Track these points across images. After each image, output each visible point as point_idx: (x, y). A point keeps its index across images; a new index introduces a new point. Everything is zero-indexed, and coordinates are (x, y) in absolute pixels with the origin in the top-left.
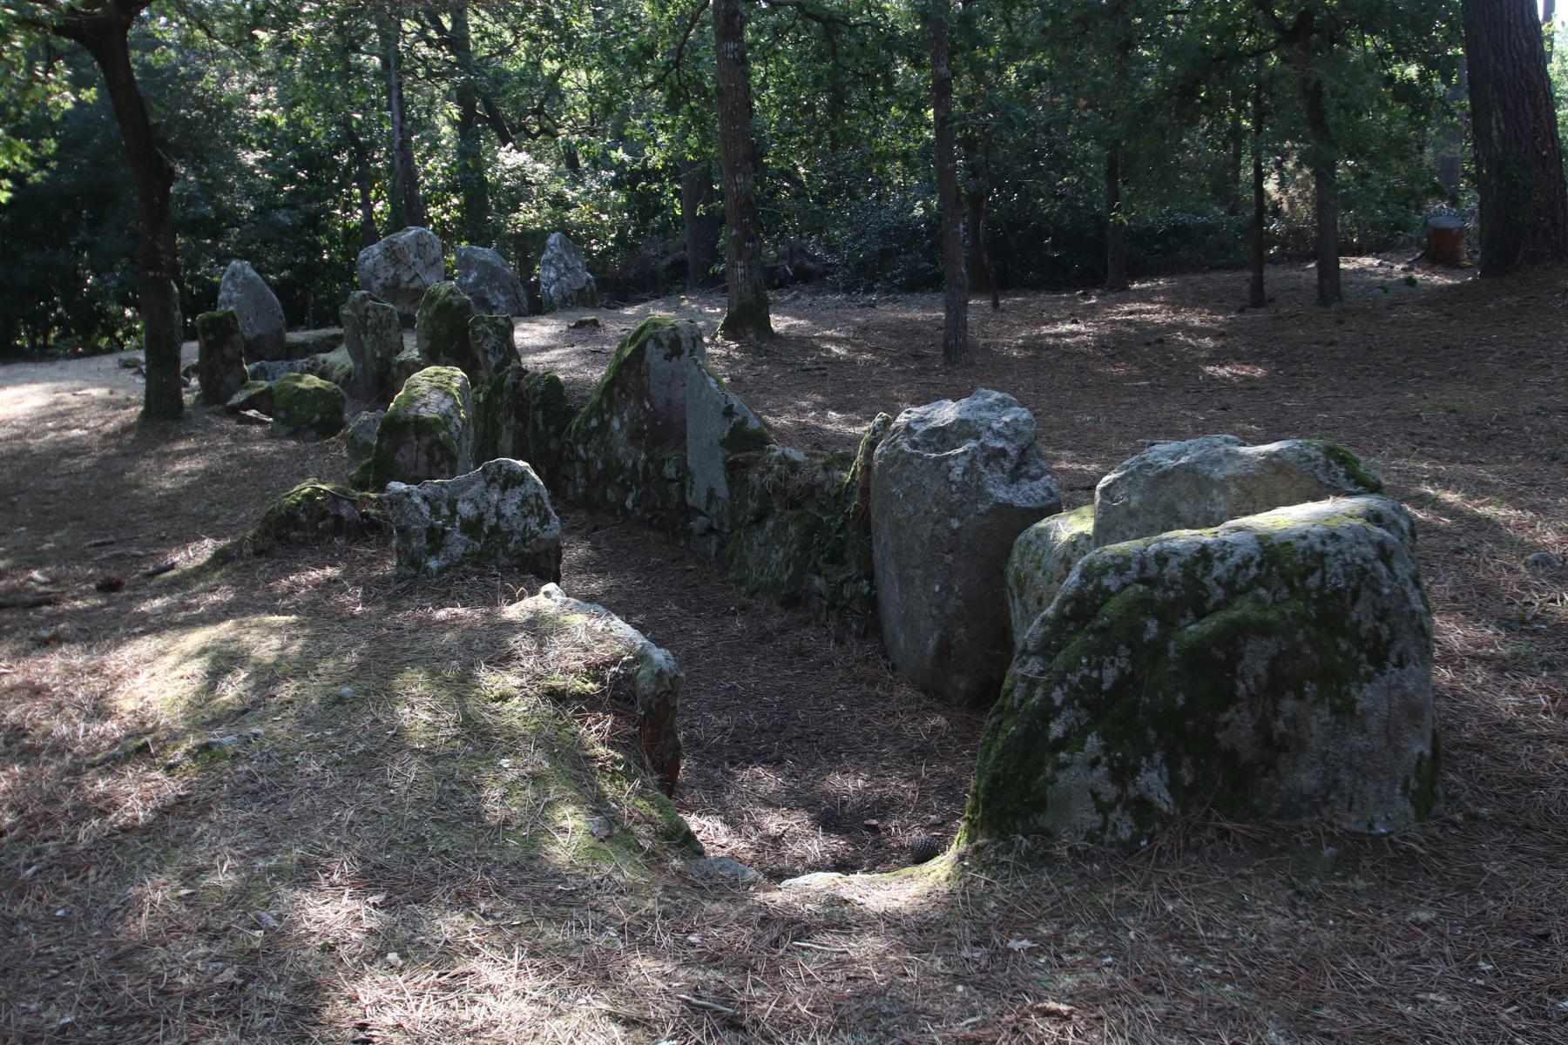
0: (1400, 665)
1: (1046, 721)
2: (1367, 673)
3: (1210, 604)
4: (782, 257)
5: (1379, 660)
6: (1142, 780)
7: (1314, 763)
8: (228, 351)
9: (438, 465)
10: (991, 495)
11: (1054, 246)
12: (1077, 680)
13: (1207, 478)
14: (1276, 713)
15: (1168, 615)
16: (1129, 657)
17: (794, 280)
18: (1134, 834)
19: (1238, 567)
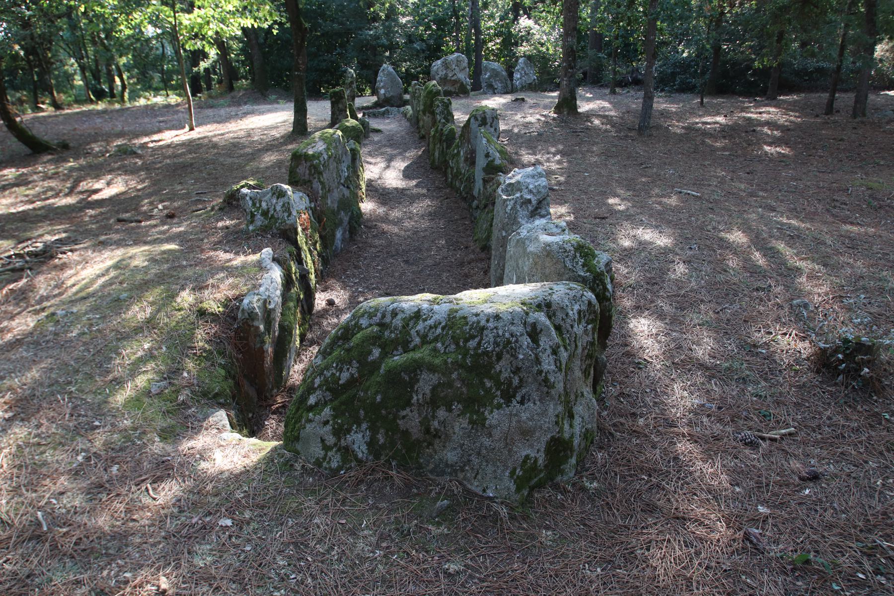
0: (522, 403)
1: (309, 394)
3: (412, 345)
4: (628, 73)
5: (508, 397)
6: (349, 438)
7: (455, 448)
8: (340, 106)
11: (752, 75)
14: (434, 417)
15: (388, 348)
17: (631, 84)
18: (339, 466)
19: (431, 327)
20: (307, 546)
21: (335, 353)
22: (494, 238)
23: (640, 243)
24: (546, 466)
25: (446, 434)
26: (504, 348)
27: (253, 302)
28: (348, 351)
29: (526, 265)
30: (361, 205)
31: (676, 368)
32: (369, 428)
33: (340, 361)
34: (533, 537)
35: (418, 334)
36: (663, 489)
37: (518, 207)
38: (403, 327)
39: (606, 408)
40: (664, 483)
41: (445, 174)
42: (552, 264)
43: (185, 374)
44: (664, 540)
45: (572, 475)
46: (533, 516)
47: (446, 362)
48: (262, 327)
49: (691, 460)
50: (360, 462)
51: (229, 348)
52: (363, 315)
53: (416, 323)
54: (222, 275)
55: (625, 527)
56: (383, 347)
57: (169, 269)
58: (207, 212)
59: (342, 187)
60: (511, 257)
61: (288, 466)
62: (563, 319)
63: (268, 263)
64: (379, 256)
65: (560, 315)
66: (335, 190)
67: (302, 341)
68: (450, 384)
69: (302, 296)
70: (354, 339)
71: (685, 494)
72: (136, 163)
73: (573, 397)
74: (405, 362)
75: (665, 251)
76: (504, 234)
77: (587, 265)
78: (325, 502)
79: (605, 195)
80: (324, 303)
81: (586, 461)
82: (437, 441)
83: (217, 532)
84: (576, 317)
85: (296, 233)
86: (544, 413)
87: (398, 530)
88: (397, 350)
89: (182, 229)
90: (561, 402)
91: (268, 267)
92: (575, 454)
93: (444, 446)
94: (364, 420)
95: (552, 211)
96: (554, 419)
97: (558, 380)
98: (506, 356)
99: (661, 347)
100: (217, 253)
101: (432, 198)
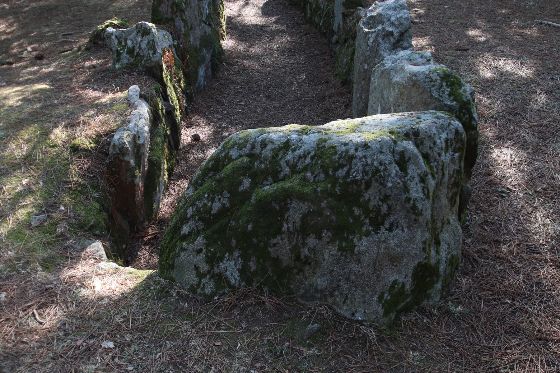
0: (390, 230)
1: (182, 224)
2: (367, 230)
5: (377, 224)
6: (222, 266)
9: (175, 13)
10: (381, 55)
12: (201, 205)
14: (304, 244)
15: (258, 178)
16: (229, 198)
18: (212, 292)
19: (300, 157)
20: (185, 366)
21: (206, 184)
22: (356, 71)
23: (502, 74)
24: (412, 291)
25: (316, 261)
26: (373, 176)
27: (124, 137)
28: (219, 181)
29: (392, 96)
30: (222, 42)
31: (539, 197)
32: (241, 256)
33: (212, 191)
34: (401, 358)
35: (287, 164)
36: (526, 312)
37: (380, 39)
38: (273, 157)
39: (470, 236)
40: (527, 306)
41: (304, 10)
42: (417, 94)
43: (62, 208)
44: (527, 360)
45: (437, 299)
46: (401, 338)
47: (315, 191)
48: (132, 162)
49: (553, 285)
50: (233, 288)
51: (102, 183)
52: (232, 147)
53: (285, 153)
54: (92, 112)
55: (490, 348)
56: (253, 177)
57: (41, 108)
58: (74, 53)
59: (203, 25)
60: (375, 88)
61: (164, 292)
62: (430, 148)
63: (136, 99)
64: (241, 93)
65: (428, 143)
66: (197, 28)
67: (169, 176)
68: (319, 213)
69: (168, 132)
70: (225, 170)
71: (547, 317)
72: (4, 8)
73: (439, 224)
74: (276, 191)
75: (525, 83)
76: (366, 67)
77: (453, 95)
78: (201, 325)
79: (466, 27)
80: (189, 139)
81: (451, 286)
82: (307, 267)
83: (101, 353)
84: (444, 145)
85: (162, 71)
86: (412, 240)
87: (271, 351)
88: (267, 180)
89: (51, 69)
90: (428, 229)
91: (136, 103)
92: (440, 279)
93: (314, 273)
94: (236, 248)
95: (414, 43)
96: (421, 246)
97: (425, 207)
98: (375, 184)
99: (524, 176)
100: (86, 91)
101: (291, 34)
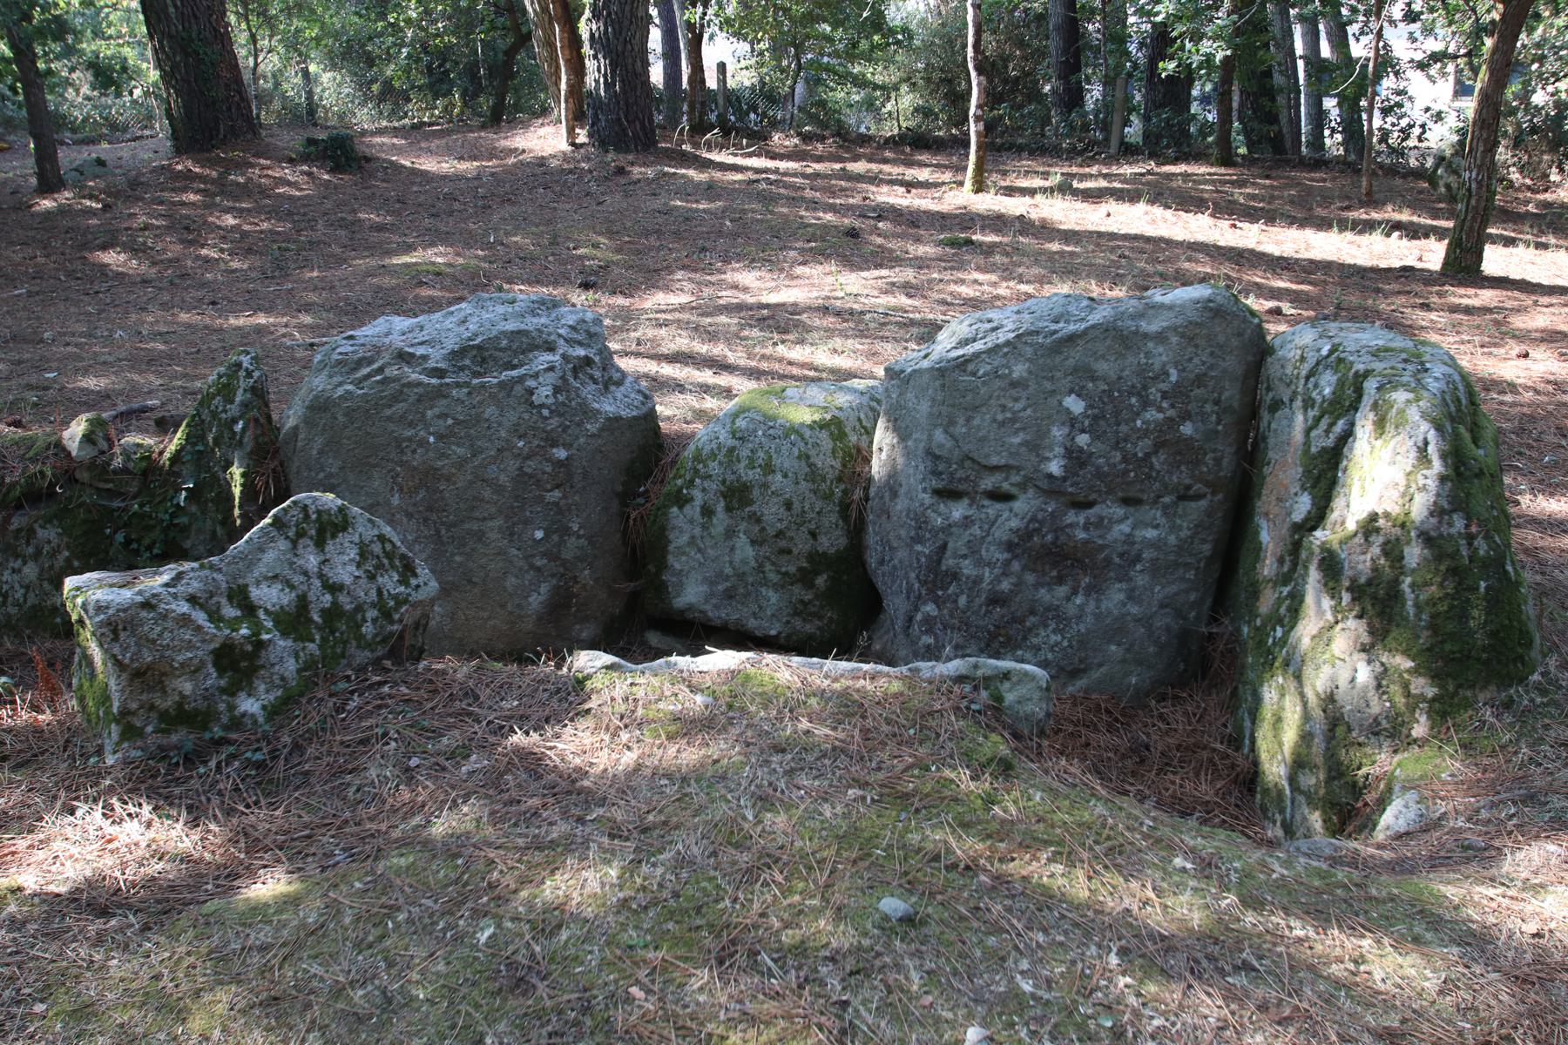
10: (598, 412)
13: (1136, 333)
